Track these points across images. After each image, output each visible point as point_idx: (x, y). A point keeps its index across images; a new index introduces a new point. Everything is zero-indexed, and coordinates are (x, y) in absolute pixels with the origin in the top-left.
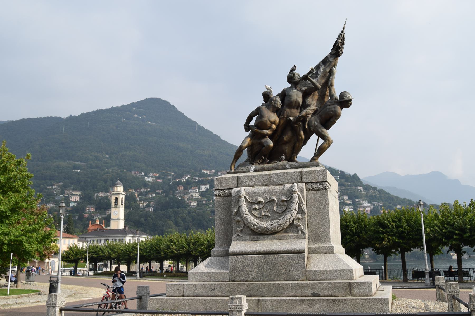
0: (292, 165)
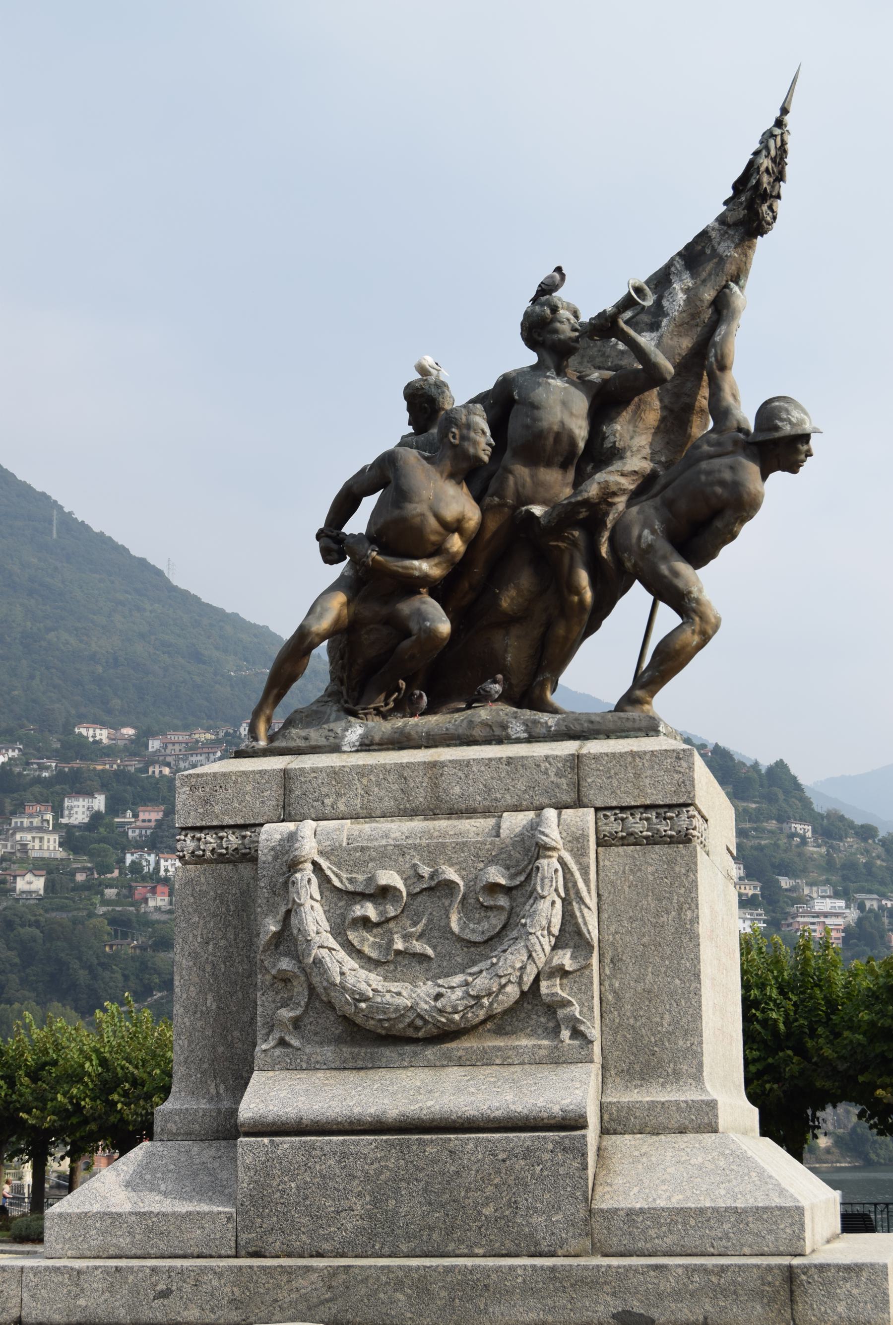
0: (535, 722)
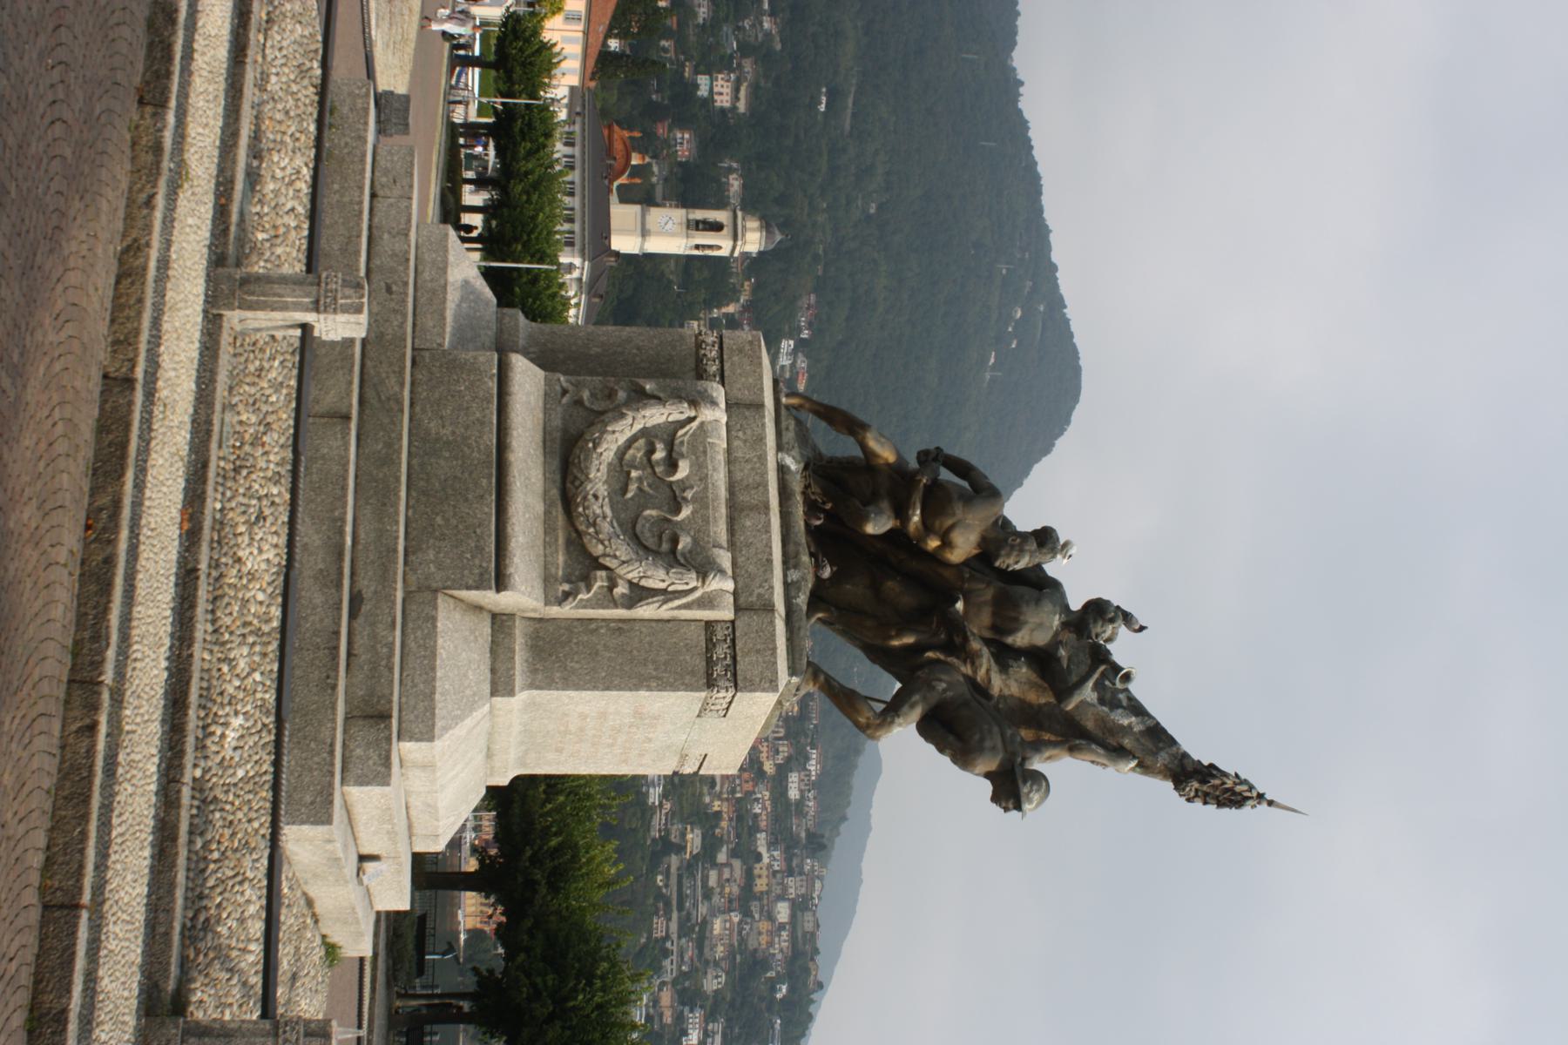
0: (799, 589)
